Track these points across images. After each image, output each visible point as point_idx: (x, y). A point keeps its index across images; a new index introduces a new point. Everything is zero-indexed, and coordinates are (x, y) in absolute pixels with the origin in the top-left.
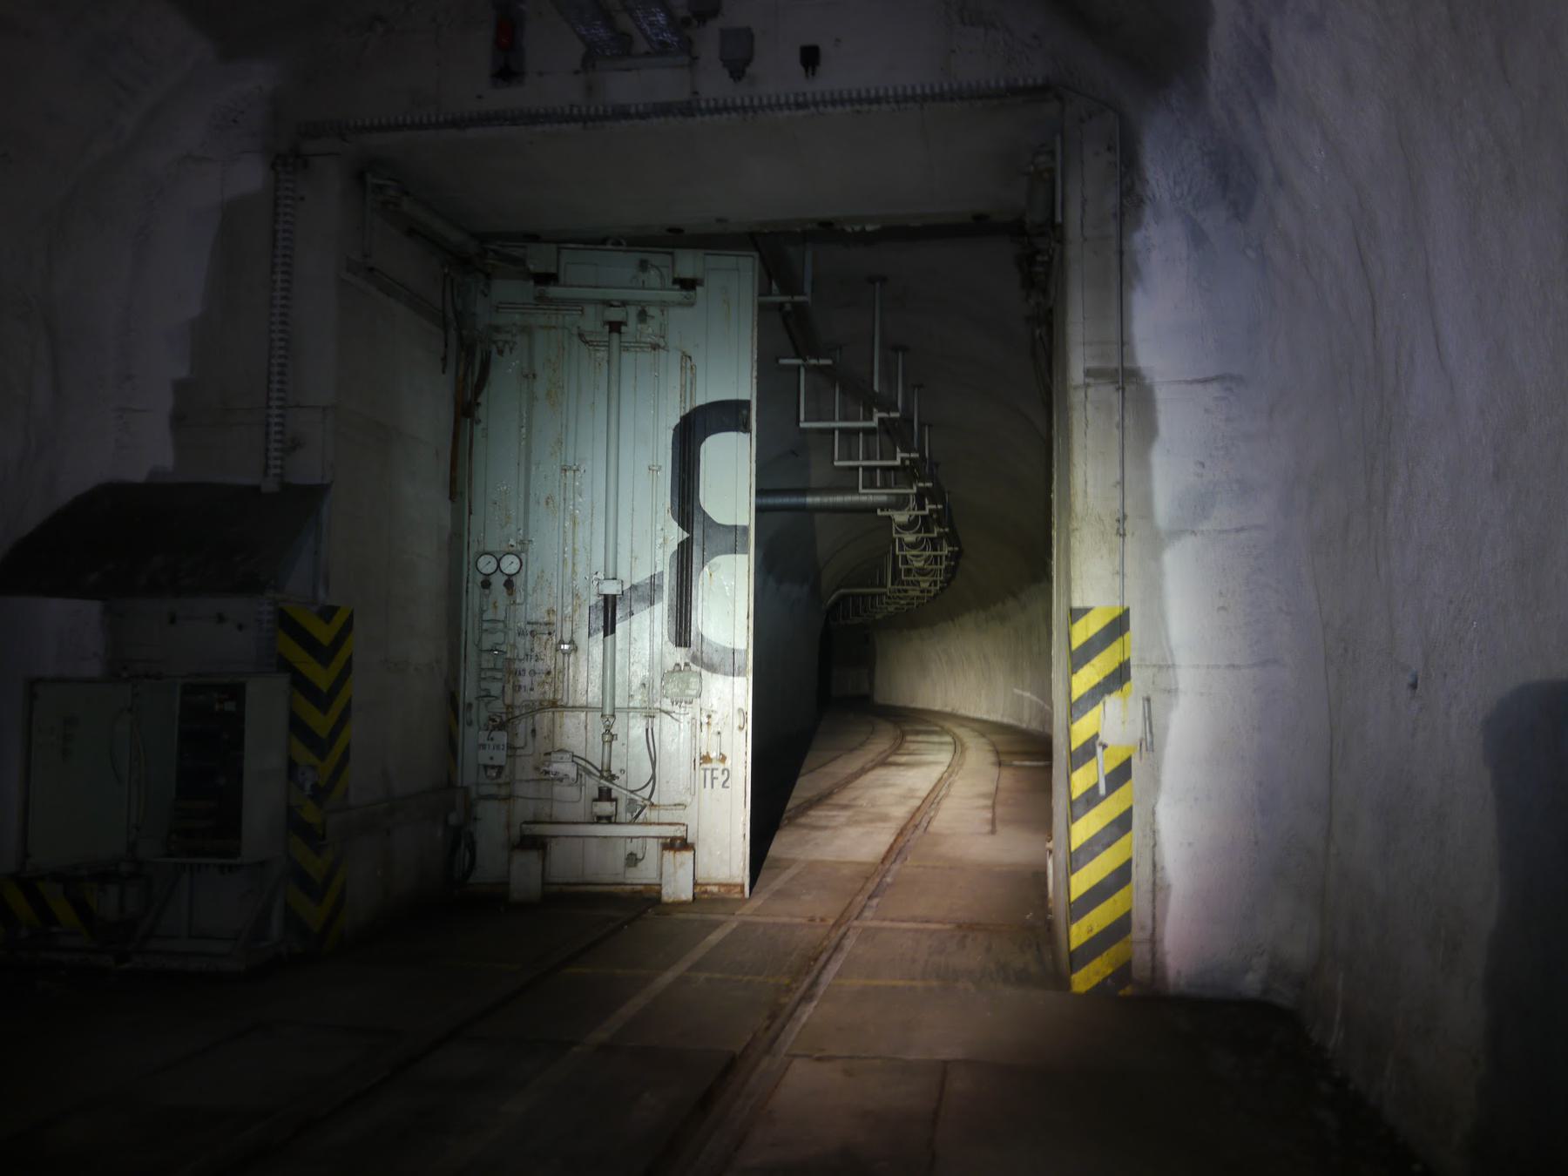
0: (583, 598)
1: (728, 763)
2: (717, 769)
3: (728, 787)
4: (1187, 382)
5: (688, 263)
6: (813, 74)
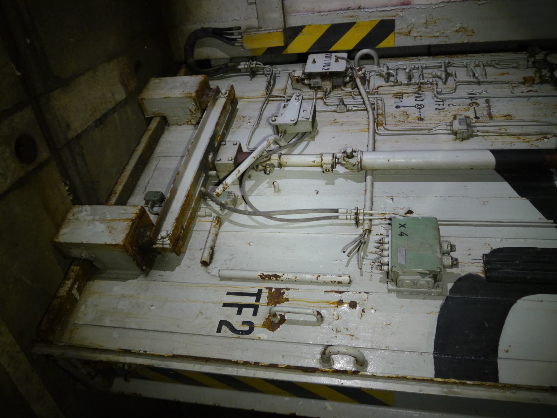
1: (260, 333)
2: (255, 314)
3: (219, 330)
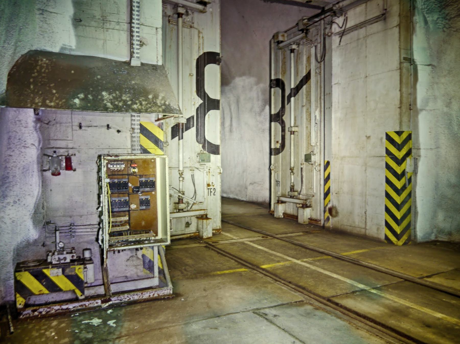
0: (169, 124)
4: (425, 65)
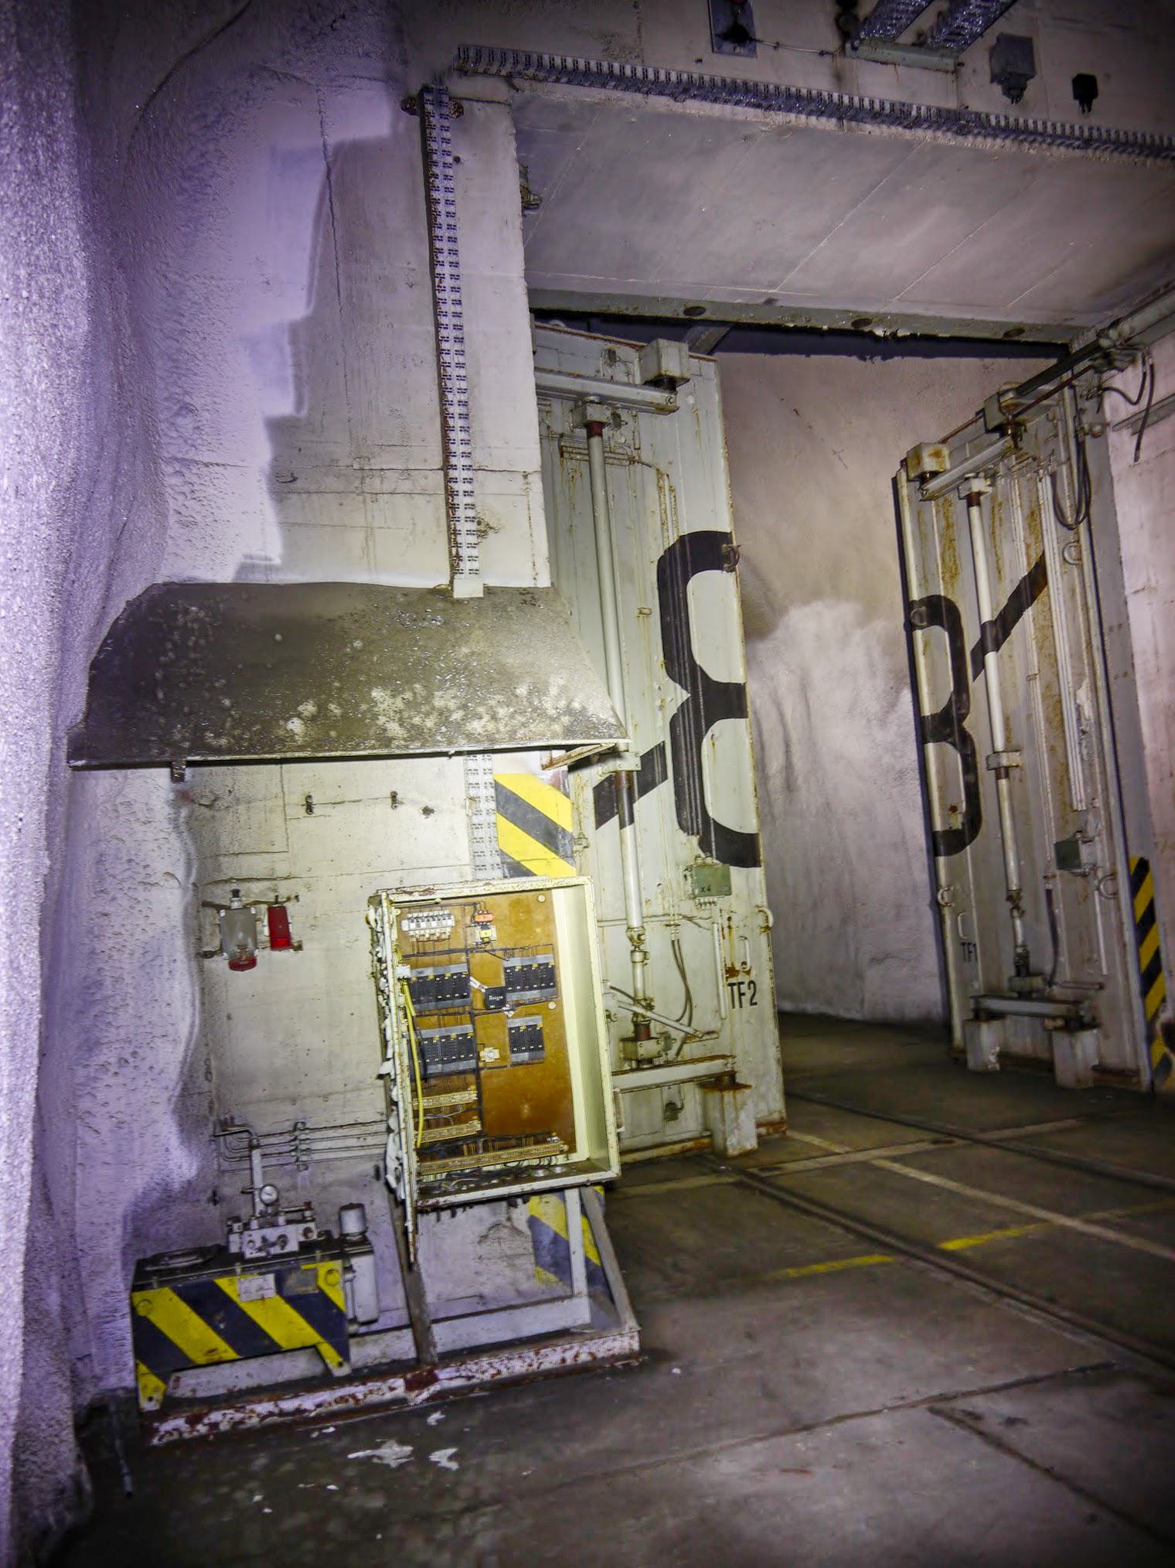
2: (743, 983)
5: (673, 358)
6: (1089, 110)
